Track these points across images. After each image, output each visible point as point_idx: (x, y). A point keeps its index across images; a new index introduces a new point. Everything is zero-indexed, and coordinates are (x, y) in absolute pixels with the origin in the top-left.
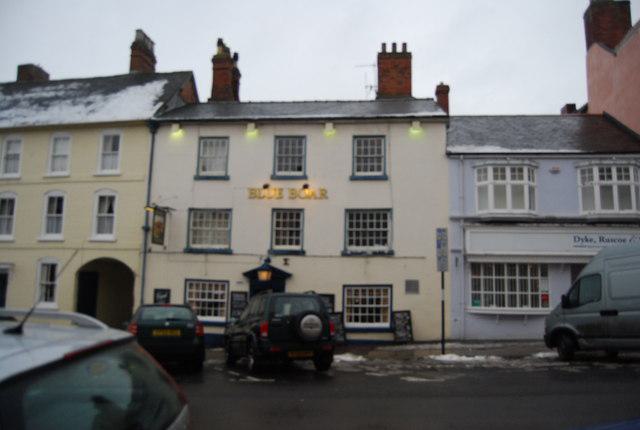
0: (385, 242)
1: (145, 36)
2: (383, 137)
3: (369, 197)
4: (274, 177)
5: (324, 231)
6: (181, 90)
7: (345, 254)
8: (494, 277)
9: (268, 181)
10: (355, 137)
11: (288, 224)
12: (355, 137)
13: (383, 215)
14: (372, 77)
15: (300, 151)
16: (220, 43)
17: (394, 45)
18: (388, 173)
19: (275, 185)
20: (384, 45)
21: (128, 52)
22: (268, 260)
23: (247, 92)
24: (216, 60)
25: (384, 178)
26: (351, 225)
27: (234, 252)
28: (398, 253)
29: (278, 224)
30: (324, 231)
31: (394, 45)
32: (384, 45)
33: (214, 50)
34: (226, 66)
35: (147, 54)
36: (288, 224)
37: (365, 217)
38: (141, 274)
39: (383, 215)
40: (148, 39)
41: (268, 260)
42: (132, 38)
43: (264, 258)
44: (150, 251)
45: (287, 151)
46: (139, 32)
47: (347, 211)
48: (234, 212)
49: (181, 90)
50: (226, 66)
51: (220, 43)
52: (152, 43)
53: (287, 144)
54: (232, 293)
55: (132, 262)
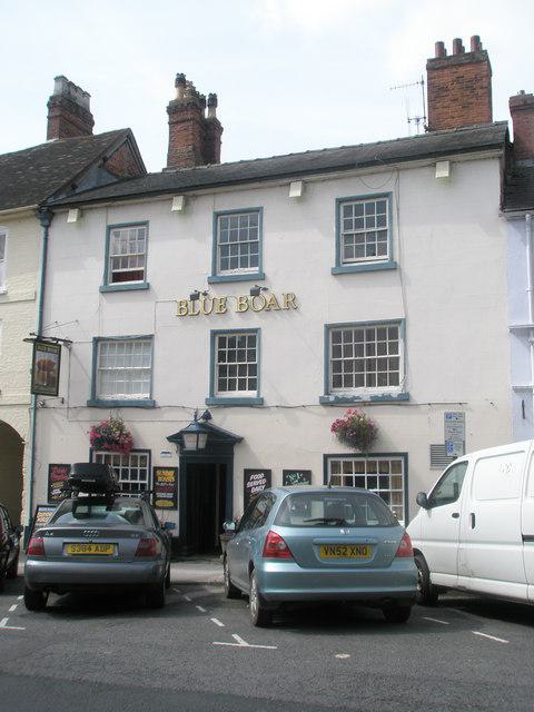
0: (253, 385)
1: (71, 84)
2: (387, 195)
3: (365, 303)
4: (215, 281)
5: (293, 365)
6: (105, 160)
7: (325, 403)
8: (365, 475)
9: (203, 287)
10: (339, 201)
11: (235, 358)
12: (339, 201)
13: (387, 333)
14: (418, 104)
15: (254, 233)
16: (181, 81)
17: (458, 42)
18: (396, 259)
19: (214, 293)
20: (440, 46)
21: (45, 111)
22: (207, 416)
23: (232, 151)
24: (173, 110)
25: (392, 267)
26: (337, 351)
27: (159, 404)
28: (417, 397)
29: (222, 356)
30: (293, 365)
31: (458, 42)
32: (440, 46)
33: (173, 94)
34: (194, 118)
35: (78, 115)
36: (235, 358)
37: (370, 337)
38: (31, 444)
39: (387, 333)
40: (77, 89)
41: (207, 416)
42: (50, 89)
43: (201, 413)
44: (44, 406)
45: (234, 238)
46: (61, 79)
47: (328, 328)
48: (263, 333)
49: (105, 160)
50: (194, 118)
51: (181, 81)
52: (86, 95)
53: (234, 225)
54: (156, 469)
55: (21, 423)
